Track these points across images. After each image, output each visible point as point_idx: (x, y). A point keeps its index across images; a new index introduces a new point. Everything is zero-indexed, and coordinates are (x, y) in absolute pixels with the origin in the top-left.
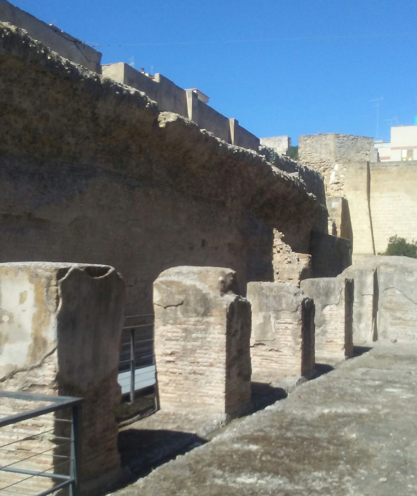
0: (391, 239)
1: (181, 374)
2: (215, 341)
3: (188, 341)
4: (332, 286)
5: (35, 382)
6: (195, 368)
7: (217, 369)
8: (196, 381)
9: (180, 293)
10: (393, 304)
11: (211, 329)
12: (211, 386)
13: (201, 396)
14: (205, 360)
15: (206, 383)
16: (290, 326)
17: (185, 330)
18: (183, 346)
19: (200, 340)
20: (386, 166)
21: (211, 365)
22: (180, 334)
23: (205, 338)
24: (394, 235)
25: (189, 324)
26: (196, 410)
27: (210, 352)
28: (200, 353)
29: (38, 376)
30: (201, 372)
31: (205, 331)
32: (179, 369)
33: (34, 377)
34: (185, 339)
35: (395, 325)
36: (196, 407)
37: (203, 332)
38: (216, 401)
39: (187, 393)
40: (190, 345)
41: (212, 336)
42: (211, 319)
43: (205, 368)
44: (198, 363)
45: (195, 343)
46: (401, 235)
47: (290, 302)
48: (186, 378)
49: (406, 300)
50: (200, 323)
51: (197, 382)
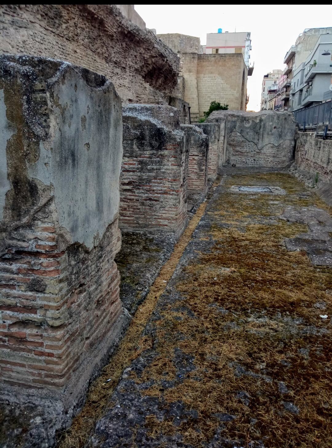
0: (212, 103)
1: (138, 200)
2: (168, 172)
3: (144, 172)
4: (209, 129)
5: (22, 247)
6: (150, 195)
7: (171, 196)
8: (151, 206)
9: (135, 128)
10: (235, 142)
11: (165, 161)
12: (165, 210)
13: (155, 218)
14: (160, 188)
15: (160, 208)
16: (196, 158)
17: (141, 162)
18: (139, 176)
19: (155, 171)
20: (208, 57)
21: (166, 193)
22: (136, 166)
23: (160, 169)
24: (214, 100)
25: (145, 157)
26: (151, 230)
27: (164, 182)
28: (154, 183)
29: (26, 240)
30: (155, 199)
31: (160, 163)
32: (135, 196)
33: (19, 240)
34: (141, 170)
35: (236, 155)
36: (152, 228)
37: (158, 164)
38: (169, 223)
39: (143, 216)
40: (145, 176)
41: (166, 167)
42: (166, 152)
43: (159, 195)
44: (153, 191)
45: (150, 174)
46: (217, 101)
47: (197, 139)
48: (143, 204)
49: (243, 139)
50: (155, 156)
51: (152, 207)
